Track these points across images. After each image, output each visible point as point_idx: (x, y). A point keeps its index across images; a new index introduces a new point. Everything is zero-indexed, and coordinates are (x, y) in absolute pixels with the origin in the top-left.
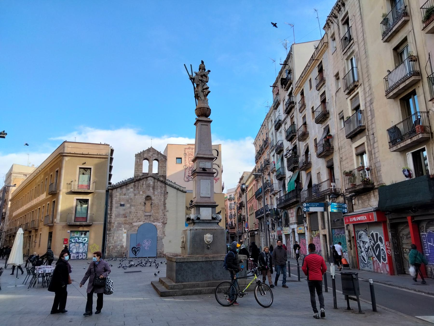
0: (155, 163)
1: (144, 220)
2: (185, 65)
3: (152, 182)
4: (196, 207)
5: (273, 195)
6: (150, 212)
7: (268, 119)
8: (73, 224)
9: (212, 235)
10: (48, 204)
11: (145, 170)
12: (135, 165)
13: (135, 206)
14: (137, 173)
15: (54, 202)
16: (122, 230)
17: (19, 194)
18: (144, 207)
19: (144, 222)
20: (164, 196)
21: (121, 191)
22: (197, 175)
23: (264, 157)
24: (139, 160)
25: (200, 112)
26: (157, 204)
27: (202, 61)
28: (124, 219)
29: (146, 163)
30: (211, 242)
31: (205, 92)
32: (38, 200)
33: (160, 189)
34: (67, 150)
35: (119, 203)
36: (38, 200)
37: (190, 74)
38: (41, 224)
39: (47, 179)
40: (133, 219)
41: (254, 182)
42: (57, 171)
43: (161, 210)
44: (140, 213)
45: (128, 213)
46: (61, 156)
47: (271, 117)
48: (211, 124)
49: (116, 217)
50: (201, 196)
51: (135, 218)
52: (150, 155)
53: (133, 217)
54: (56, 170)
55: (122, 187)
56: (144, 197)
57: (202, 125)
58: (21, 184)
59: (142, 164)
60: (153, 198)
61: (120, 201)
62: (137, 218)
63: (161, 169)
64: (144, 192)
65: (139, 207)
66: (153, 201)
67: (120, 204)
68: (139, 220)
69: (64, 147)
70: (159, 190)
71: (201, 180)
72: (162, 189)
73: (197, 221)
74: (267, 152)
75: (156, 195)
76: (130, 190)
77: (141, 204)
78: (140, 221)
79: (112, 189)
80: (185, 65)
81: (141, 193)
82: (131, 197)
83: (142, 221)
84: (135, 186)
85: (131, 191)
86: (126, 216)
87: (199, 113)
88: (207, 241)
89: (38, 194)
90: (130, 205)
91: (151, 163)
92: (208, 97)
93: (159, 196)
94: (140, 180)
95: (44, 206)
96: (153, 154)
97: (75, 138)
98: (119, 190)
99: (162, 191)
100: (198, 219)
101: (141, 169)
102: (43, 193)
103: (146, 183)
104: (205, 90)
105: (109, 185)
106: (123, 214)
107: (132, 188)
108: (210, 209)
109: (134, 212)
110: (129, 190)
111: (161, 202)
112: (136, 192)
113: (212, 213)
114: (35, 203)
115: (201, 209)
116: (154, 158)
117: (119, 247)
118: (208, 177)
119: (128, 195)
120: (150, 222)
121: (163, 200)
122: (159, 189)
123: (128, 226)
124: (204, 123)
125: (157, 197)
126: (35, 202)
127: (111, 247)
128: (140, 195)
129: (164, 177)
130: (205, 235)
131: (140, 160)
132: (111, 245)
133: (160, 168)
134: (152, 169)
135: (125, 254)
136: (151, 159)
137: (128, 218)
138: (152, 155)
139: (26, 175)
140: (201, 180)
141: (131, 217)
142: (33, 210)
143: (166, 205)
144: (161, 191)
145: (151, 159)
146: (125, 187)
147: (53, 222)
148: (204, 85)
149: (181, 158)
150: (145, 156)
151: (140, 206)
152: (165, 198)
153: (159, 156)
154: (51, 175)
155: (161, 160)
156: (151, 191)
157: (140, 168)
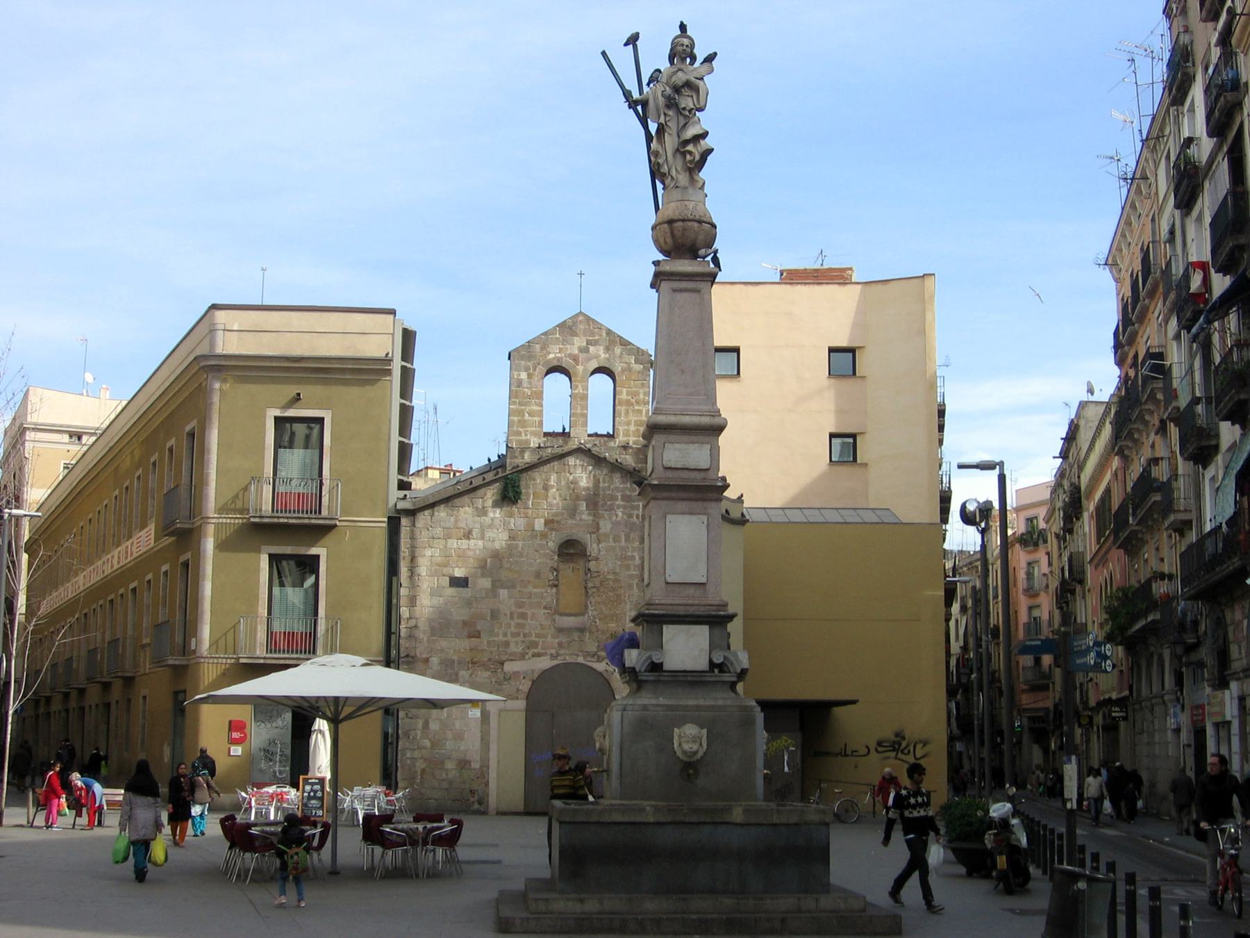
0: (600, 386)
1: (553, 651)
2: (604, 54)
3: (584, 475)
4: (647, 622)
5: (1175, 530)
6: (583, 614)
7: (1155, 146)
8: (262, 661)
9: (705, 731)
10: (166, 573)
11: (555, 417)
13: (514, 587)
15: (186, 565)
17: (58, 523)
19: (553, 657)
21: (452, 519)
22: (653, 499)
23: (1145, 338)
24: (524, 375)
27: (682, 23)
28: (465, 644)
29: (556, 387)
30: (700, 754)
31: (690, 153)
32: (127, 552)
33: (624, 507)
34: (228, 345)
35: (445, 570)
36: (127, 552)
37: (632, 86)
38: (145, 656)
39: (154, 464)
40: (507, 644)
41: (1116, 462)
42: (192, 435)
43: (628, 606)
44: (538, 618)
45: (486, 620)
46: (203, 367)
47: (1165, 138)
49: (433, 634)
50: (669, 580)
51: (513, 639)
52: (576, 352)
53: (505, 635)
54: (188, 428)
55: (457, 501)
56: (551, 544)
57: (674, 290)
58: (61, 478)
59: (539, 395)
60: (593, 549)
61: (446, 565)
62: (523, 642)
63: (627, 413)
65: (530, 588)
66: (592, 565)
67: (448, 579)
68: (531, 649)
69: (212, 331)
70: (620, 514)
72: (633, 508)
73: (651, 677)
74: (1156, 314)
75: (607, 535)
77: (538, 575)
78: (538, 655)
79: (412, 513)
80: (604, 54)
83: (545, 654)
86: (479, 632)
87: (666, 242)
88: (685, 752)
89: (125, 530)
90: (494, 582)
91: (580, 390)
92: (704, 174)
93: (619, 541)
95: (149, 582)
96: (589, 343)
97: (263, 270)
98: (442, 513)
100: (656, 667)
102: (143, 526)
103: (558, 482)
104: (690, 147)
105: (402, 493)
106: (465, 623)
108: (702, 632)
109: (511, 614)
111: (628, 568)
113: (713, 647)
114: (116, 567)
115: (669, 631)
116: (594, 365)
117: (450, 765)
118: (694, 505)
119: (483, 538)
120: (581, 660)
122: (619, 507)
124: (684, 285)
125: (613, 544)
126: (115, 561)
127: (420, 765)
130: (676, 729)
131: (530, 376)
132: (417, 754)
133: (623, 408)
135: (476, 797)
136: (580, 368)
137: (484, 640)
138: (584, 350)
139: (79, 438)
140: (669, 517)
141: (497, 635)
142: (112, 596)
144: (630, 516)
145: (580, 368)
146: (466, 499)
147: (185, 650)
148: (685, 124)
149: (736, 350)
150: (554, 354)
153: (618, 350)
154: (171, 450)
155: (623, 370)
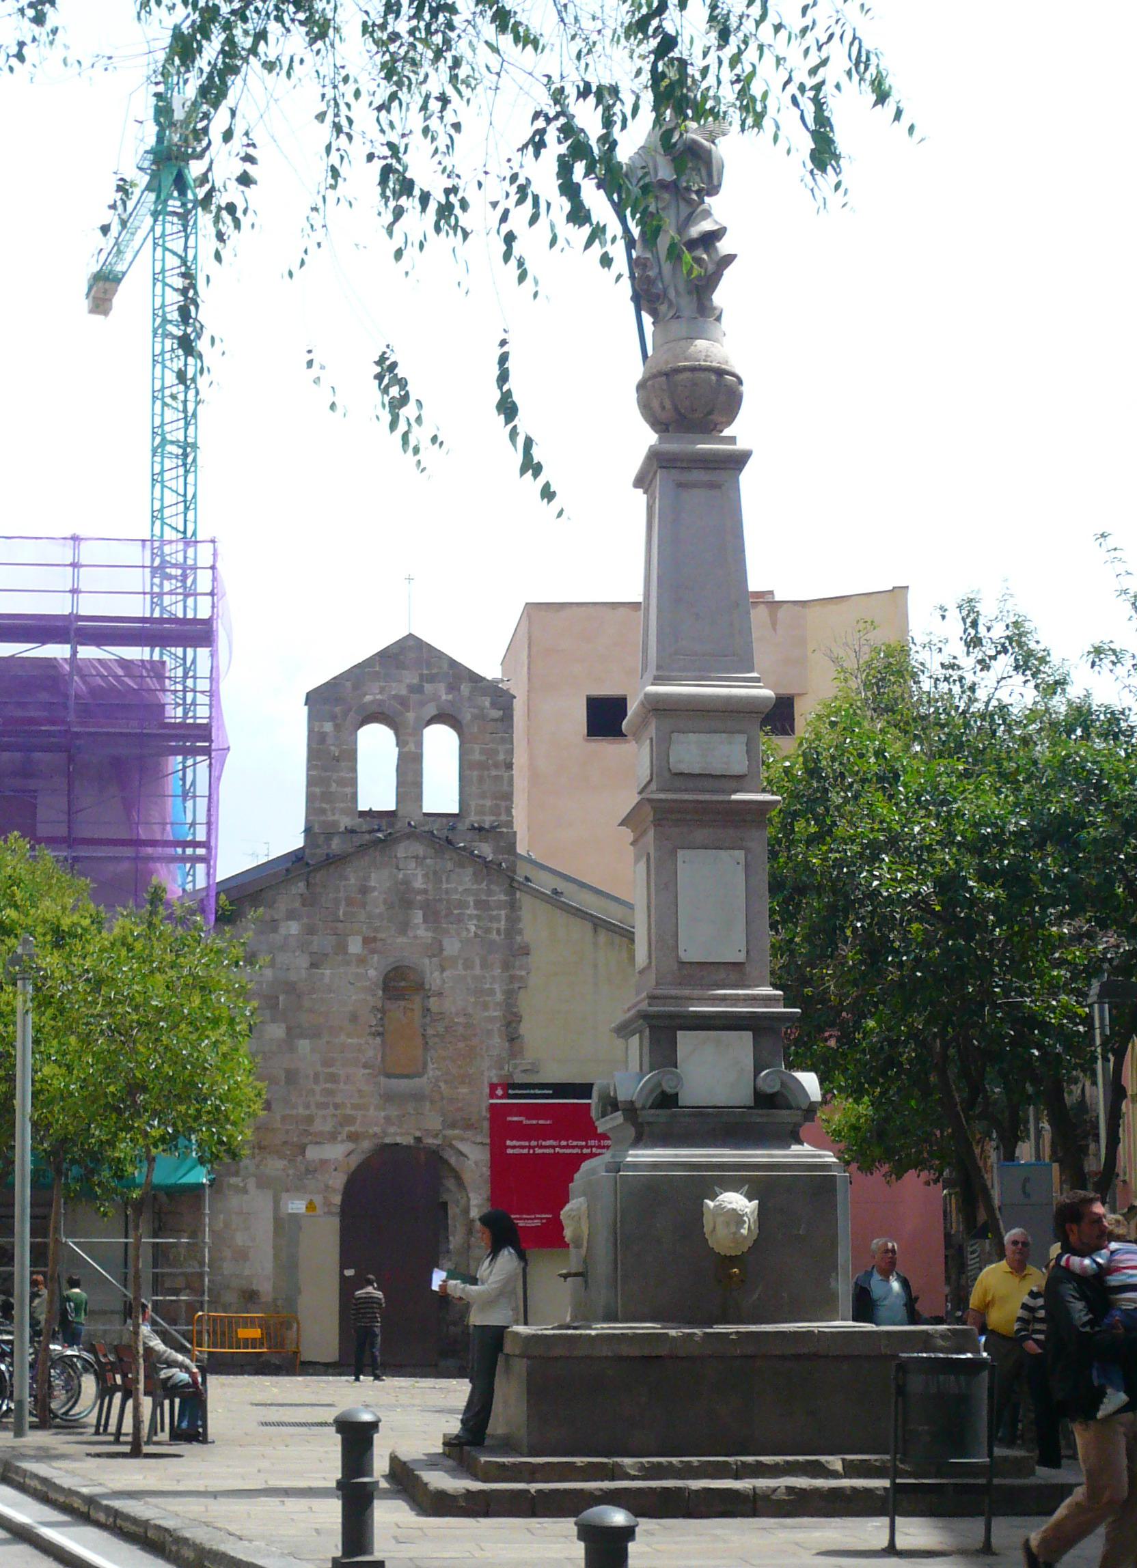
3: (420, 873)
12: (309, 760)
14: (323, 811)
16: (245, 1191)
18: (378, 1040)
20: (506, 966)
24: (328, 727)
25: (668, 404)
26: (461, 1020)
33: (478, 918)
48: (747, 478)
51: (321, 1113)
53: (307, 1106)
56: (372, 973)
60: (434, 979)
64: (375, 939)
70: (473, 928)
71: (680, 853)
76: (283, 931)
77: (354, 1018)
81: (355, 946)
82: (293, 976)
84: (309, 901)
85: (286, 937)
87: (663, 408)
93: (472, 968)
94: (334, 861)
99: (494, 936)
100: (667, 1100)
101: (348, 790)
107: (291, 915)
109: (316, 1076)
110: (275, 930)
111: (485, 1007)
112: (321, 942)
116: (431, 710)
121: (499, 997)
122: (471, 917)
123: (280, 1164)
128: (348, 963)
129: (501, 835)
131: (337, 727)
134: (418, 785)
136: (411, 716)
140: (680, 853)
143: (524, 1029)
151: (349, 1036)
152: (512, 978)
156: (421, 932)
157: (342, 783)
